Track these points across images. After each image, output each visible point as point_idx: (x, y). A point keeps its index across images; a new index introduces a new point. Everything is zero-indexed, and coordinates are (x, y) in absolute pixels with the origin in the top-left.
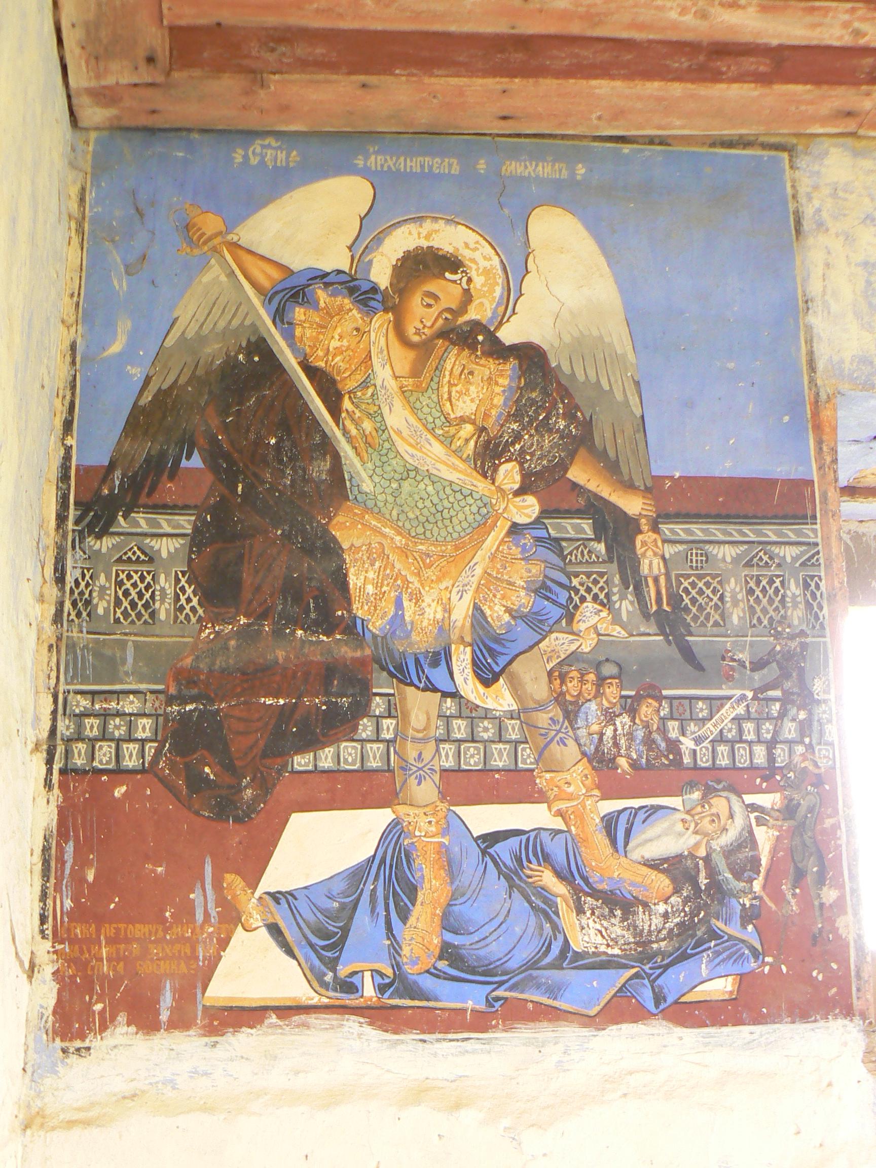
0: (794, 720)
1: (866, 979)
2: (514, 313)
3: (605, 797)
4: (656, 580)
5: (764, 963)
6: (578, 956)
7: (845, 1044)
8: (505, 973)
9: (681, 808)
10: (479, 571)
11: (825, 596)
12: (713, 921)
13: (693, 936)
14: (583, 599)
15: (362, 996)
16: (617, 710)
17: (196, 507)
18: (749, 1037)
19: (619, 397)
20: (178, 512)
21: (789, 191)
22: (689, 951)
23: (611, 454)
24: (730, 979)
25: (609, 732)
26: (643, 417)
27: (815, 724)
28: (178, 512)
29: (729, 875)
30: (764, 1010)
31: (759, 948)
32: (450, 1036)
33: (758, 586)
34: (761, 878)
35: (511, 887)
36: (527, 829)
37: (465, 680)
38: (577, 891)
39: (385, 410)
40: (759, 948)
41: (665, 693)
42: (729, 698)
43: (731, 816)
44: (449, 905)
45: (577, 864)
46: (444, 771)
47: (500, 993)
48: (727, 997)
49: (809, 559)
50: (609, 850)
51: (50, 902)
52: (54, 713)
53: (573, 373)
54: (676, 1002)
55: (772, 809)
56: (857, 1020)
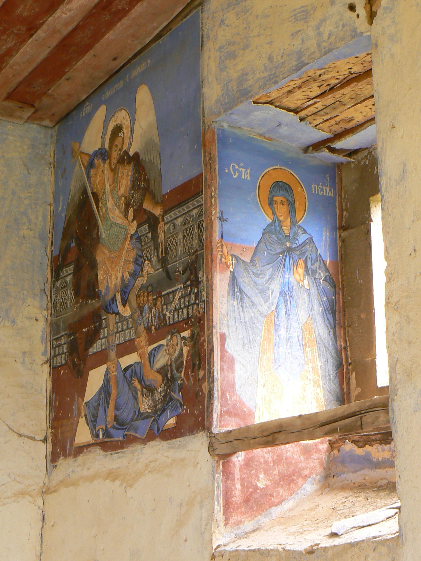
0: (194, 293)
1: (210, 411)
2: (132, 141)
3: (150, 345)
4: (162, 243)
5: (183, 409)
6: (142, 414)
7: (202, 443)
8: (127, 425)
9: (165, 344)
10: (123, 259)
11: (204, 229)
12: (172, 394)
13: (166, 400)
14: (145, 261)
15: (100, 439)
16: (152, 306)
17: (145, 221)
18: (179, 443)
19: (155, 163)
20: (53, 274)
21: (201, 26)
22: (165, 407)
23: (154, 191)
24: (175, 417)
25: (150, 317)
26: (161, 169)
27: (200, 293)
28: (53, 274)
29: (175, 371)
30: (183, 431)
31: (182, 402)
32: (117, 451)
33: (148, 252)
34: (184, 370)
35: (129, 389)
36: (133, 364)
37: (120, 306)
38: (142, 387)
39: (107, 201)
40: (182, 402)
41: (163, 293)
42: (177, 290)
43: (177, 344)
44: (116, 399)
45: (218, 366)
46: (117, 345)
47: (126, 433)
48: (173, 426)
49: (200, 213)
50: (149, 368)
51: (50, 415)
52: (50, 348)
53: (145, 160)
54: (162, 430)
55: (188, 337)
56: (206, 432)
